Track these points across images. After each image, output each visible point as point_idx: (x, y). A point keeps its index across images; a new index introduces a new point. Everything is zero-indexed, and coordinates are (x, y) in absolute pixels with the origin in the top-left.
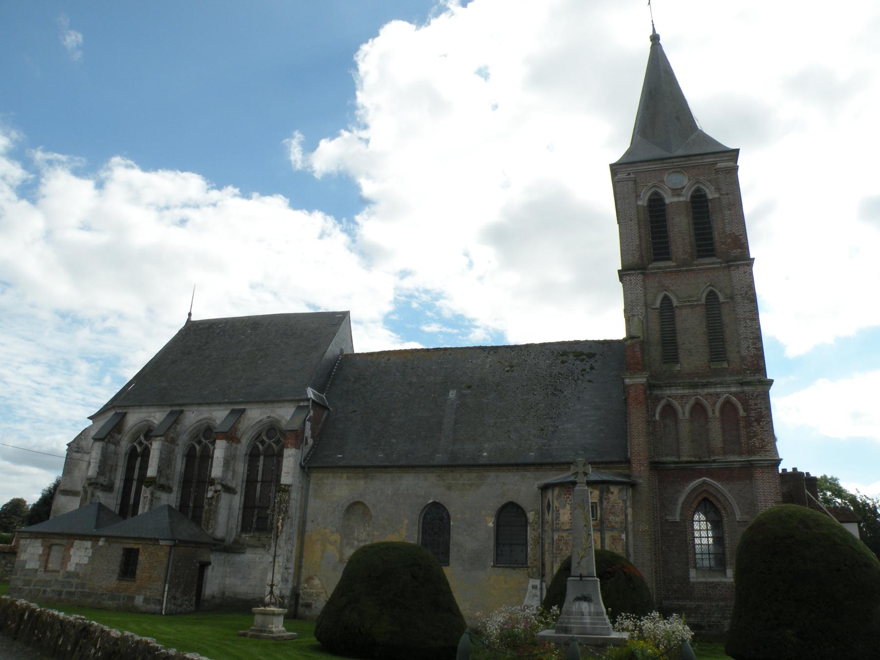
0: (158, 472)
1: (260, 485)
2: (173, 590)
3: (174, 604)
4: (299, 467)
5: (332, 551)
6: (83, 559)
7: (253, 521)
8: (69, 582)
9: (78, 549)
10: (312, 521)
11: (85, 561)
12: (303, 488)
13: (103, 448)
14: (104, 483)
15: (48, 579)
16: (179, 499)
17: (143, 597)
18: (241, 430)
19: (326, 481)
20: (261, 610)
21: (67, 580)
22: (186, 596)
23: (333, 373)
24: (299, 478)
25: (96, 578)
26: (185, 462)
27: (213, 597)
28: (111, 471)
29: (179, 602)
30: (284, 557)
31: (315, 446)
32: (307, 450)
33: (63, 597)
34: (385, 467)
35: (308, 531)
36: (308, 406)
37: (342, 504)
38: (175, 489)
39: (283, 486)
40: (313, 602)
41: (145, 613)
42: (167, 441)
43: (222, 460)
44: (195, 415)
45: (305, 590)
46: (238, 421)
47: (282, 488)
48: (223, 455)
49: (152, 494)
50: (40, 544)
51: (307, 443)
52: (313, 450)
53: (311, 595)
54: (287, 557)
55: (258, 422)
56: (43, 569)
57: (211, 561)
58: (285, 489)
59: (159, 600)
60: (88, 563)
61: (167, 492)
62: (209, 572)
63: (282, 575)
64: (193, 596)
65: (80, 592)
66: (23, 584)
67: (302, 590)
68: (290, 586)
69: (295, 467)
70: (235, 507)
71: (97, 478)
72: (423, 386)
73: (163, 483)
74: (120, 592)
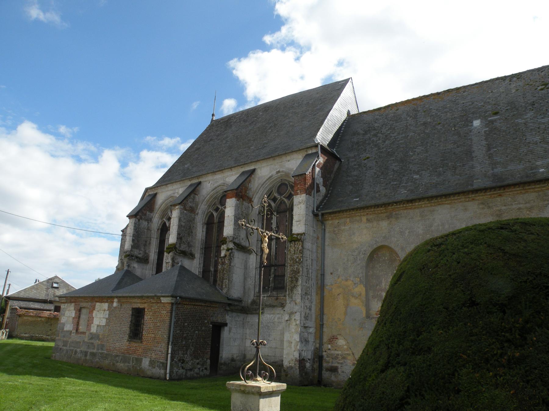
0: (177, 238)
1: (275, 242)
2: (180, 352)
3: (183, 368)
4: (311, 215)
5: (358, 306)
6: (102, 320)
7: (270, 280)
8: (92, 344)
9: (98, 311)
10: (331, 274)
11: (103, 322)
12: (318, 238)
13: (135, 224)
14: (139, 256)
15: (78, 340)
16: (202, 265)
17: (149, 359)
18: (252, 190)
19: (344, 228)
20: (240, 385)
21: (91, 341)
22: (198, 359)
23: (342, 131)
24: (313, 227)
25: (112, 339)
26: (205, 230)
27: (233, 360)
28: (145, 245)
29: (189, 366)
30: (301, 314)
31: (329, 195)
32: (320, 198)
33: (88, 358)
34: (412, 201)
35: (327, 285)
36: (317, 153)
37: (364, 251)
38: (197, 255)
39: (295, 236)
40: (339, 366)
41: (151, 378)
42: (186, 210)
43: (233, 218)
44: (211, 184)
45: (329, 352)
46: (248, 180)
47: (294, 237)
48: (233, 214)
49: (173, 259)
50: (73, 308)
51: (318, 191)
52: (327, 199)
53: (336, 357)
54: (306, 314)
55: (267, 180)
56: (75, 331)
57: (227, 322)
58: (297, 238)
59: (163, 363)
60: (106, 325)
61: (189, 258)
62: (225, 333)
63: (300, 334)
64: (207, 359)
65: (100, 353)
66: (63, 344)
67: (326, 351)
68: (311, 347)
69: (306, 214)
70: (251, 267)
71: (131, 250)
72: (440, 124)
73: (184, 250)
74: (130, 354)
